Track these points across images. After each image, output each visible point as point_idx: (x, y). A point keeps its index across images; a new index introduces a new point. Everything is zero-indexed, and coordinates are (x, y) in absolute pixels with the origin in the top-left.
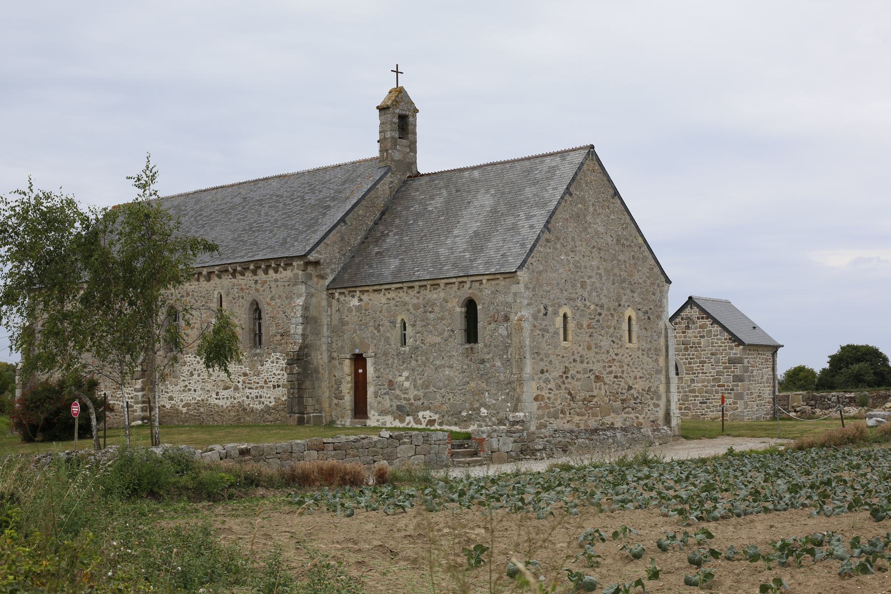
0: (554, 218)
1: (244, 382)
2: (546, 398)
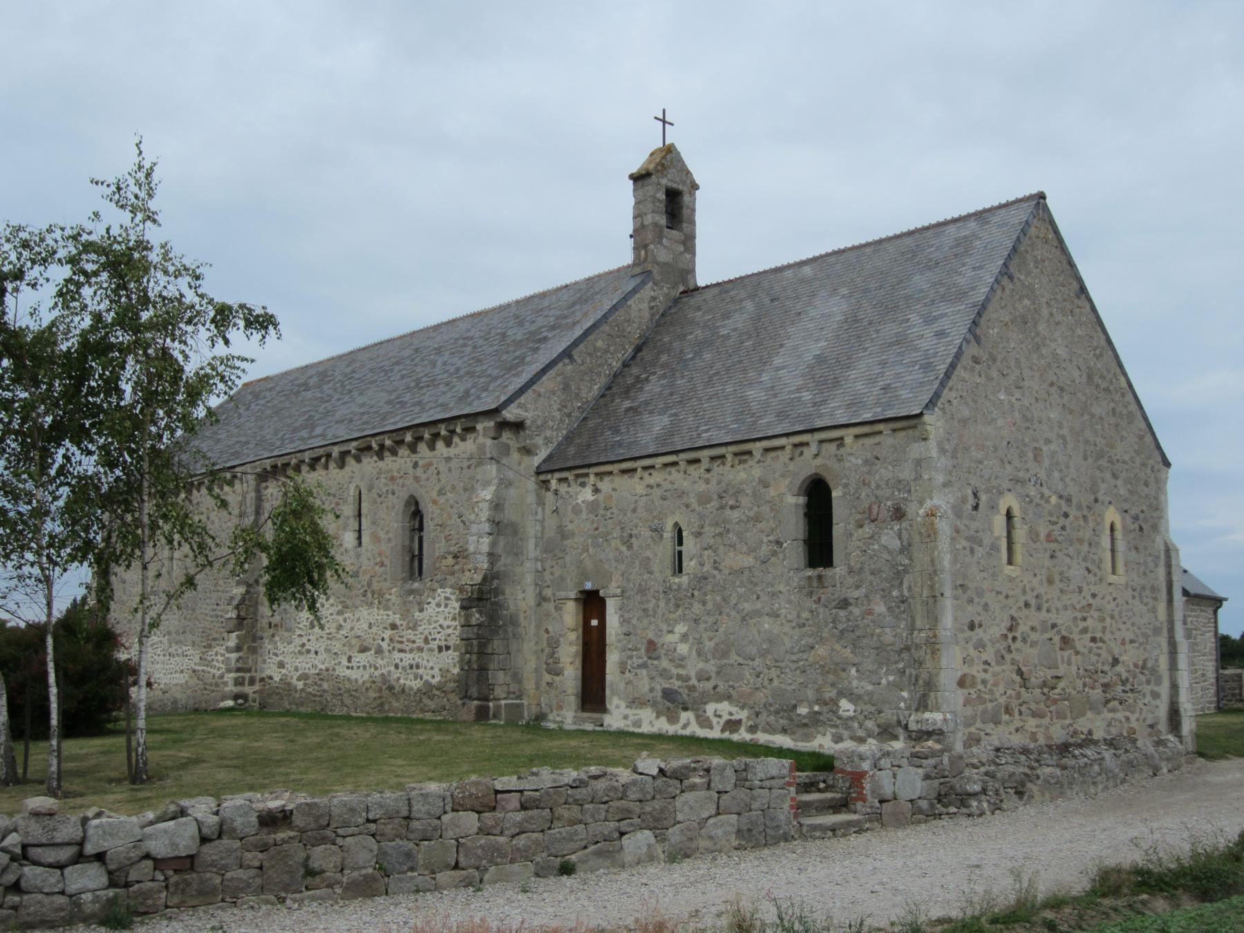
0: (984, 317)
1: (391, 640)
2: (979, 681)
